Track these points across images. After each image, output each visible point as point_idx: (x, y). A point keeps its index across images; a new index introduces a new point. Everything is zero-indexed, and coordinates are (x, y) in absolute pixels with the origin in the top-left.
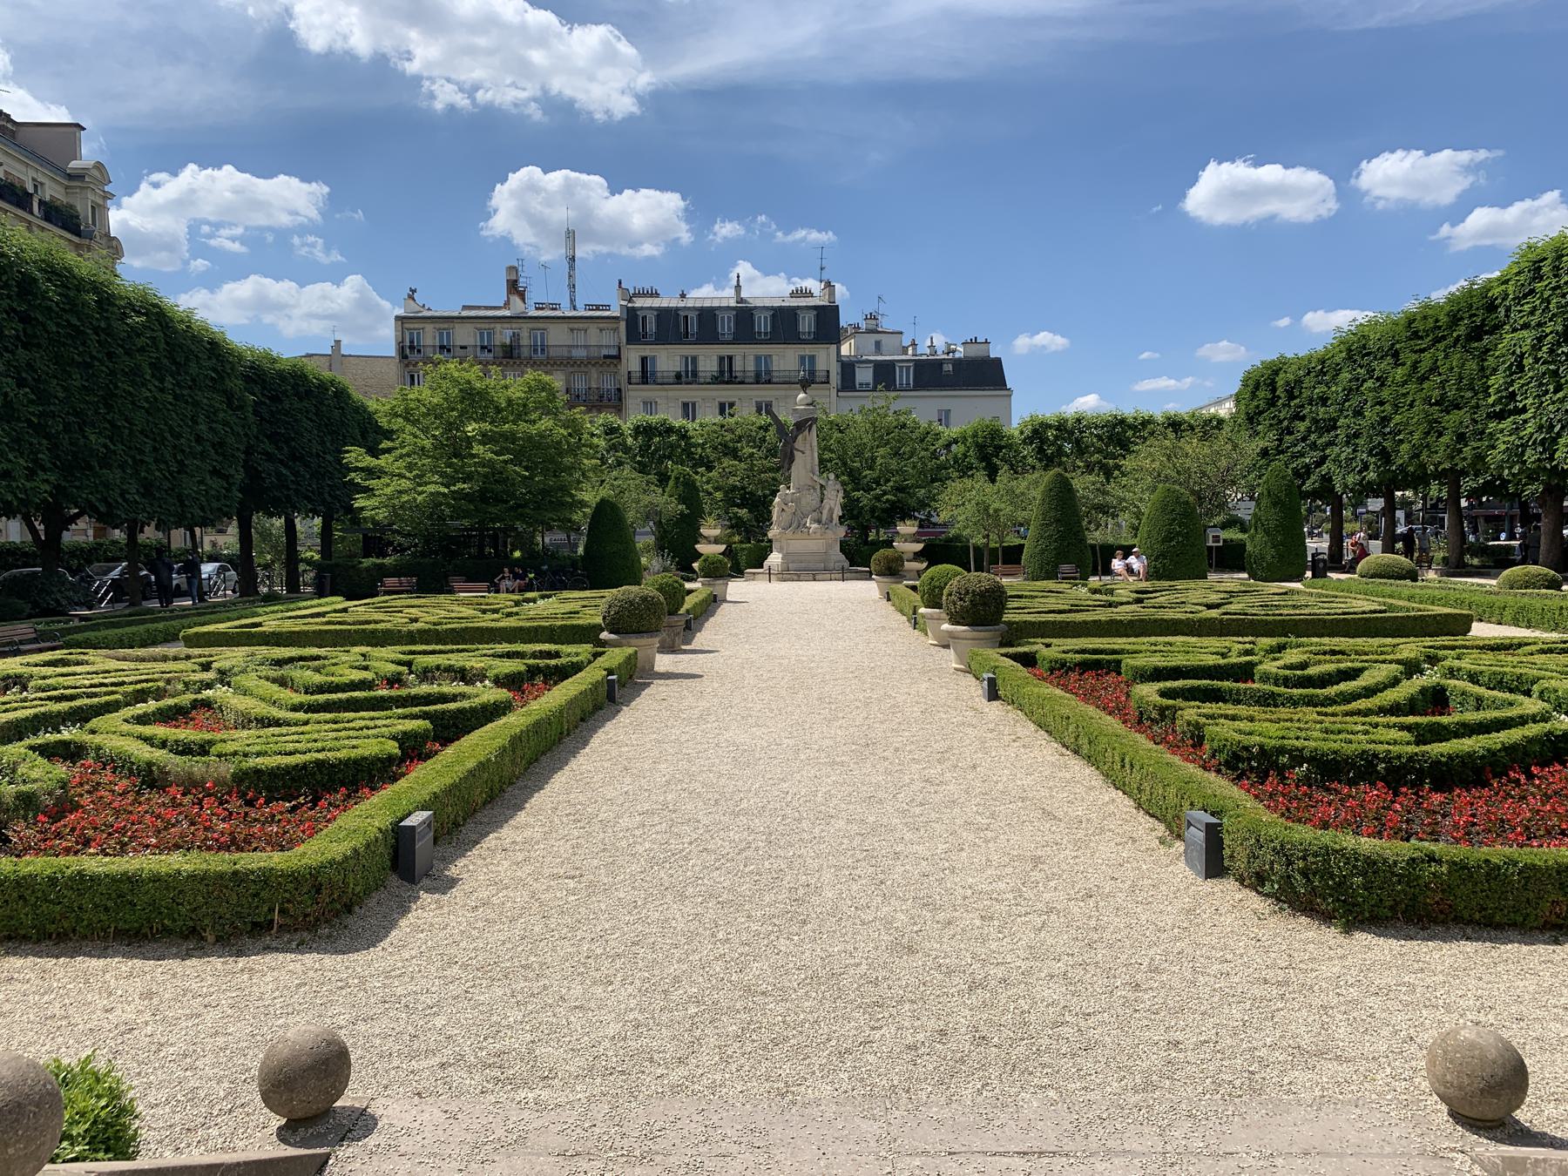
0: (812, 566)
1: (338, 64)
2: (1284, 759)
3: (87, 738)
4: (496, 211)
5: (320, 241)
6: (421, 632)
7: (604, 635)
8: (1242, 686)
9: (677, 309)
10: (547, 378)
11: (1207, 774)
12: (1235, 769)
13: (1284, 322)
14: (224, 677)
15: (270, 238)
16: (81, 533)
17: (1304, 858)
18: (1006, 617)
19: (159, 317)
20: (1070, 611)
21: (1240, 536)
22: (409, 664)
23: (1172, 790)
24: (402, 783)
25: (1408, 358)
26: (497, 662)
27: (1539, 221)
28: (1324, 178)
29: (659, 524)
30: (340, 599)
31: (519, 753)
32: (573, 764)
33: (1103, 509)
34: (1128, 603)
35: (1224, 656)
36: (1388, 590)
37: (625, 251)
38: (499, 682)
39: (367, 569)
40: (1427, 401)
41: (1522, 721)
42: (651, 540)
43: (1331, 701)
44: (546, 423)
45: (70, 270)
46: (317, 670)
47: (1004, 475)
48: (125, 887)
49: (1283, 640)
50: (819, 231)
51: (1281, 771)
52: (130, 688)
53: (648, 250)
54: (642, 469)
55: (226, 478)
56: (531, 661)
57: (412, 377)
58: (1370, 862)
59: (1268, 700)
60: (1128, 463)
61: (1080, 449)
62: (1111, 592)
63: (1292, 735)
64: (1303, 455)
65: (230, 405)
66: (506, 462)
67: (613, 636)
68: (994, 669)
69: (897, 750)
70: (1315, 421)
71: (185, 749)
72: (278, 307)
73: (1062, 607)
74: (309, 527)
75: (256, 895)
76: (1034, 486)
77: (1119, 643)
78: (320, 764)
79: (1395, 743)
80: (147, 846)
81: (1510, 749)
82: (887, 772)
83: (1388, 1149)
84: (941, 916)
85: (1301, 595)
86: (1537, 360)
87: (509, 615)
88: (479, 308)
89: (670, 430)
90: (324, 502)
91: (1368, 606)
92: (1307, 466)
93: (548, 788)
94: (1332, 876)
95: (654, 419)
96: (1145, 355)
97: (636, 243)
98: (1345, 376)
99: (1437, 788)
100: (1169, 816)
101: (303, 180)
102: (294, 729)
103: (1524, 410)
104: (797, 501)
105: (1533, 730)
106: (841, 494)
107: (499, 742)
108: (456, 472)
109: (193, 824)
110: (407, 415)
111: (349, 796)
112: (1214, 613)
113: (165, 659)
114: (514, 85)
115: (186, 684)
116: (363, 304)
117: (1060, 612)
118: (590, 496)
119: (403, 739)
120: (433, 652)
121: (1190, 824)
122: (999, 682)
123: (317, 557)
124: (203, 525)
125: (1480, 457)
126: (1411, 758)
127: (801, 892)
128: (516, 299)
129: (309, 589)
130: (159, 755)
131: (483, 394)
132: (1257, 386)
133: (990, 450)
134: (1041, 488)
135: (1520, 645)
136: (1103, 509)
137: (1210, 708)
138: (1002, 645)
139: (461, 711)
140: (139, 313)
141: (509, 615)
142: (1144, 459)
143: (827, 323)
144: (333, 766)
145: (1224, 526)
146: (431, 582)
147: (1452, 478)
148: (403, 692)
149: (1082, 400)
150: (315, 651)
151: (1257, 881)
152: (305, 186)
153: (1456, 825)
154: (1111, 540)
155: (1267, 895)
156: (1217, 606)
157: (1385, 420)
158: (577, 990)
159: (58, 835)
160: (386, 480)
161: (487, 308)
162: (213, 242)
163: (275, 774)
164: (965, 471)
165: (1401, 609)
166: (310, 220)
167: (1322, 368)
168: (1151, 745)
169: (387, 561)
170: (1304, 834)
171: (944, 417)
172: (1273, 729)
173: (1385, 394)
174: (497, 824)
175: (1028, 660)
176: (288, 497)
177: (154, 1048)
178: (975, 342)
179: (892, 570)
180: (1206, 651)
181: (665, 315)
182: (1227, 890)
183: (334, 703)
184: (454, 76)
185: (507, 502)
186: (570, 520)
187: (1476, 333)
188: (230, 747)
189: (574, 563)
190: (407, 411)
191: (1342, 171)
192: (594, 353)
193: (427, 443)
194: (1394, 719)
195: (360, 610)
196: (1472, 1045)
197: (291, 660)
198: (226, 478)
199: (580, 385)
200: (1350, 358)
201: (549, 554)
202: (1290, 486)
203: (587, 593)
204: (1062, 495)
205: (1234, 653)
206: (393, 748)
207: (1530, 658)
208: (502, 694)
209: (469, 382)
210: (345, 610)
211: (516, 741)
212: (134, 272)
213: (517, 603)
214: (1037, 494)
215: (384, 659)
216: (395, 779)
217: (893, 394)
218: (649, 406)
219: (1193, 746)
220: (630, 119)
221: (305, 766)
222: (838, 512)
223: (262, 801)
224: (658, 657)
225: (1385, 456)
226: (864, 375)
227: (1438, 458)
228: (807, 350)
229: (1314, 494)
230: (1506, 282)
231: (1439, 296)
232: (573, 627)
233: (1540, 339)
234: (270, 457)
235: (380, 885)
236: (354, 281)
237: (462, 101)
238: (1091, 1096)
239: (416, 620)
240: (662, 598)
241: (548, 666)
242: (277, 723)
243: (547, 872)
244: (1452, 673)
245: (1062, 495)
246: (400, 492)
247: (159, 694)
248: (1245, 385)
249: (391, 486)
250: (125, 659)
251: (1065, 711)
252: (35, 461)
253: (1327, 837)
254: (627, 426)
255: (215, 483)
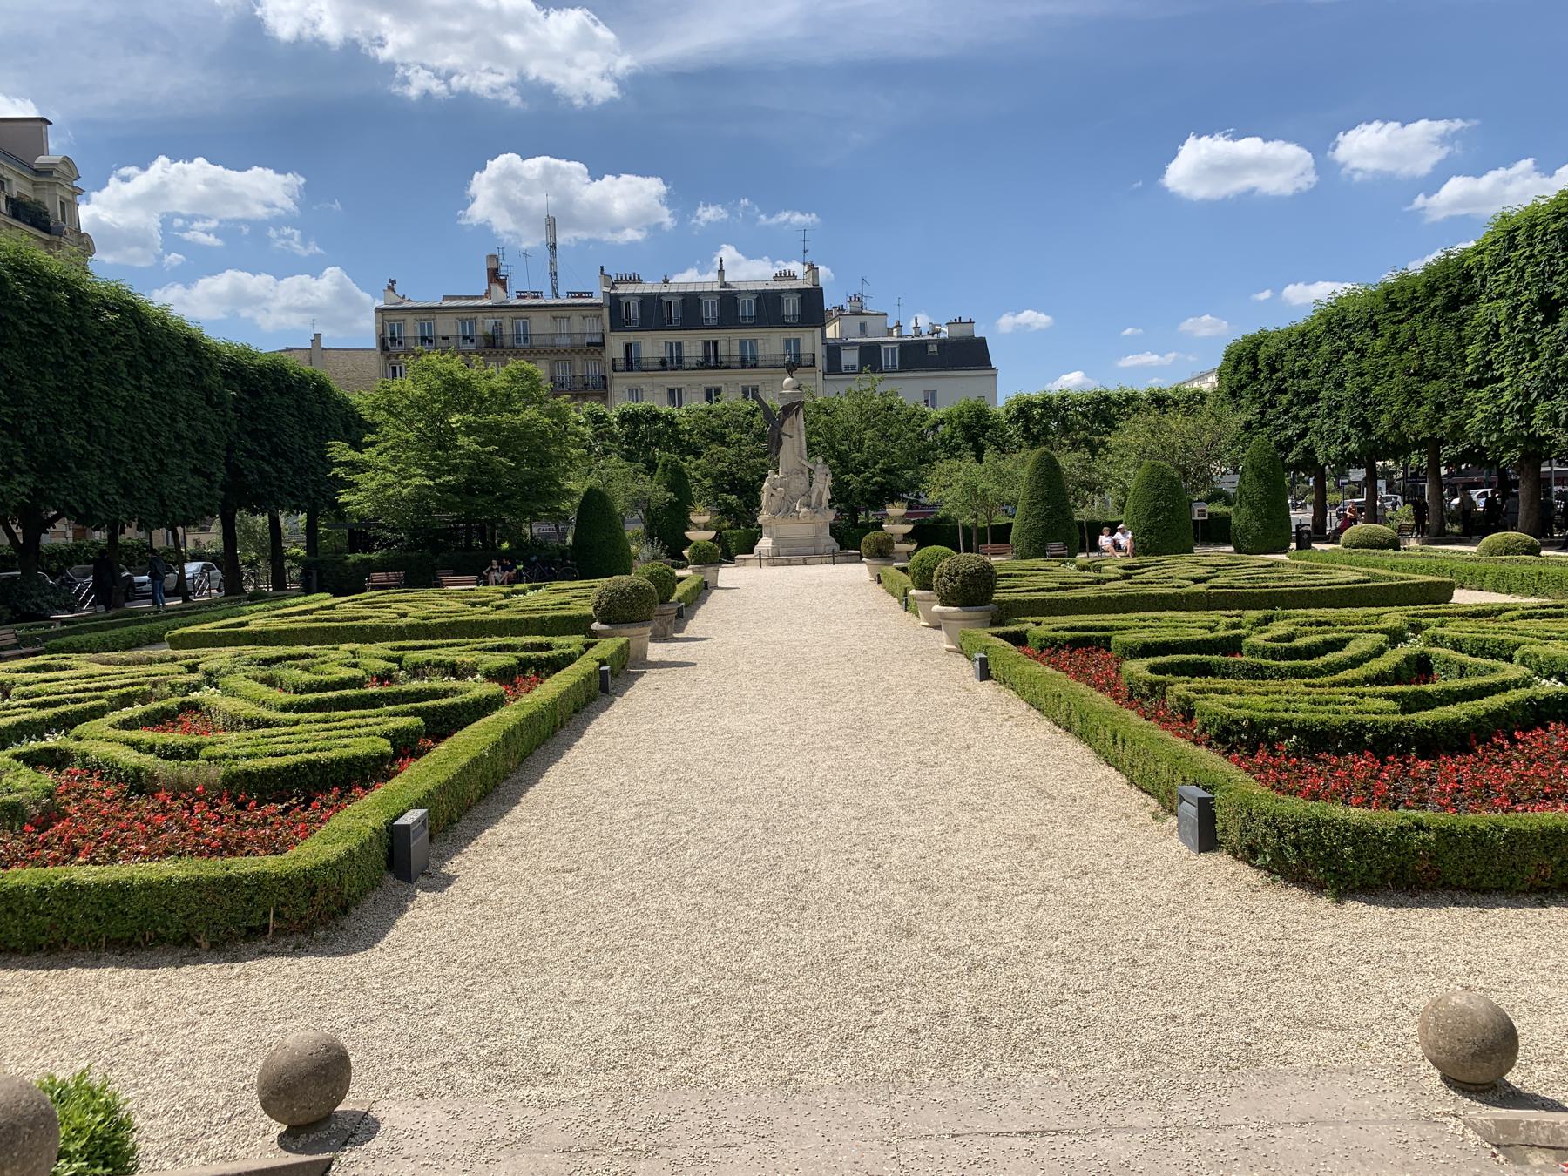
0: (801, 550)
1: (307, 54)
2: (1274, 732)
3: (73, 745)
4: (474, 200)
5: (297, 232)
6: (410, 627)
7: (596, 626)
8: (1231, 659)
9: (660, 295)
10: (529, 367)
11: (1198, 749)
12: (1225, 742)
13: (1266, 295)
14: (211, 678)
15: (246, 231)
16: (60, 535)
17: (1295, 830)
18: (997, 597)
19: (133, 314)
20: (1059, 589)
21: (1225, 509)
22: (399, 660)
23: (1164, 766)
24: (396, 782)
25: (1387, 329)
26: (488, 656)
27: (1513, 189)
28: (1302, 151)
29: (647, 511)
30: (327, 595)
31: (513, 747)
32: (568, 756)
33: (1091, 486)
34: (1116, 579)
35: (1212, 629)
36: (1371, 559)
37: (607, 236)
38: (490, 676)
39: (354, 565)
40: (1406, 371)
41: (1505, 687)
42: (640, 528)
43: (1317, 672)
44: (530, 413)
45: (40, 268)
46: (306, 669)
47: (990, 455)
48: (116, 897)
49: (1270, 612)
50: (803, 213)
51: (1271, 743)
52: (115, 693)
53: (631, 235)
54: (630, 457)
55: (208, 476)
56: (523, 654)
57: (394, 369)
58: (1360, 832)
59: (1255, 673)
60: (1113, 440)
61: (1066, 428)
62: (1099, 569)
63: (1280, 707)
64: (1285, 428)
65: (209, 401)
66: (491, 453)
67: (604, 627)
68: (985, 649)
69: (891, 732)
70: (1297, 394)
71: (172, 753)
72: (257, 301)
73: (1050, 585)
74: (293, 523)
75: (251, 899)
76: (1021, 465)
77: (1108, 619)
78: (311, 764)
79: (1382, 712)
80: (138, 853)
81: (1493, 715)
82: (882, 755)
83: (1383, 1116)
84: (939, 898)
85: (1286, 567)
86: (1512, 329)
87: (499, 607)
88: (460, 298)
89: (657, 417)
90: (308, 498)
91: (1353, 577)
92: (1289, 439)
93: (543, 781)
94: (1323, 847)
95: (640, 406)
96: (1129, 331)
97: (617, 229)
98: (1325, 348)
99: (1425, 754)
100: (1162, 792)
101: (277, 172)
102: (284, 730)
103: (1501, 378)
104: (786, 486)
105: (1515, 695)
106: (830, 478)
107: (492, 737)
108: (441, 464)
109: (183, 829)
110: (390, 408)
111: (342, 796)
112: (1201, 587)
113: (150, 661)
114: (490, 70)
115: (173, 687)
116: (343, 296)
117: (1049, 590)
118: (577, 485)
119: (395, 736)
120: (423, 648)
121: (1182, 799)
122: (991, 662)
123: (302, 553)
124: (186, 523)
125: (1458, 426)
126: (1397, 727)
127: (799, 878)
128: (497, 288)
129: (296, 586)
130: (147, 760)
131: (466, 385)
132: (1239, 361)
133: (976, 430)
134: (1028, 467)
135: (1501, 612)
136: (1091, 486)
137: (1199, 682)
138: (993, 624)
139: (453, 707)
140: (113, 311)
141: (499, 607)
142: (1128, 435)
143: (811, 306)
144: (325, 766)
145: (1209, 500)
146: (420, 576)
147: (1432, 446)
148: (394, 689)
149: (1066, 377)
150: (303, 649)
151: (1250, 854)
152: (280, 178)
153: (1442, 792)
154: (1098, 517)
155: (1259, 867)
156: (1204, 580)
157: (1365, 391)
158: (578, 984)
159: (46, 845)
160: (370, 474)
161: (468, 298)
162: (186, 236)
163: (267, 775)
164: (953, 452)
165: (1384, 578)
166: (288, 212)
167: (1303, 340)
168: (1142, 721)
169: (374, 556)
170: (1295, 806)
171: (931, 398)
172: (1261, 701)
173: (1365, 365)
174: (492, 820)
175: (1019, 639)
176: (271, 494)
177: (150, 1058)
178: (958, 322)
179: (882, 552)
180: (1194, 625)
181: (648, 301)
182: (1220, 863)
183: (324, 702)
184: (428, 62)
185: (493, 493)
186: (558, 510)
187: (1454, 303)
188: (219, 750)
189: (563, 553)
190: (390, 404)
191: (1320, 144)
192: (578, 340)
193: (411, 436)
194: (1380, 689)
195: (347, 607)
196: (1463, 1011)
197: (279, 659)
198: (208, 476)
199: (564, 373)
200: (1329, 330)
201: (536, 545)
202: (1273, 460)
203: (578, 584)
204: (1049, 473)
205: (1222, 627)
206: (385, 746)
207: (1510, 624)
208: (494, 688)
209: (451, 373)
210: (332, 607)
211: (509, 735)
212: (106, 269)
213: (507, 596)
214: (1024, 473)
215: (374, 655)
216: (388, 777)
217: (879, 376)
218: (635, 393)
219: (1184, 721)
220: (611, 103)
221: (296, 767)
222: (827, 495)
223: (253, 803)
224: (651, 645)
225: (1366, 427)
226: (850, 358)
227: (1418, 427)
228: (793, 333)
229: (1297, 467)
230: (1482, 252)
231: (1416, 267)
232: (565, 618)
233: (1516, 308)
234: (251, 454)
235: (376, 884)
236: (333, 273)
237: (437, 87)
238: (1092, 1073)
239: (404, 615)
240: (653, 587)
241: (539, 659)
242: (267, 724)
243: (544, 866)
244: (1435, 641)
245: (1049, 473)
246: (386, 486)
247: (145, 698)
248: (1227, 359)
249: (376, 480)
250: (109, 663)
251: (1057, 690)
252: (11, 463)
253: (1317, 809)
254: (613, 415)
255: (197, 481)
